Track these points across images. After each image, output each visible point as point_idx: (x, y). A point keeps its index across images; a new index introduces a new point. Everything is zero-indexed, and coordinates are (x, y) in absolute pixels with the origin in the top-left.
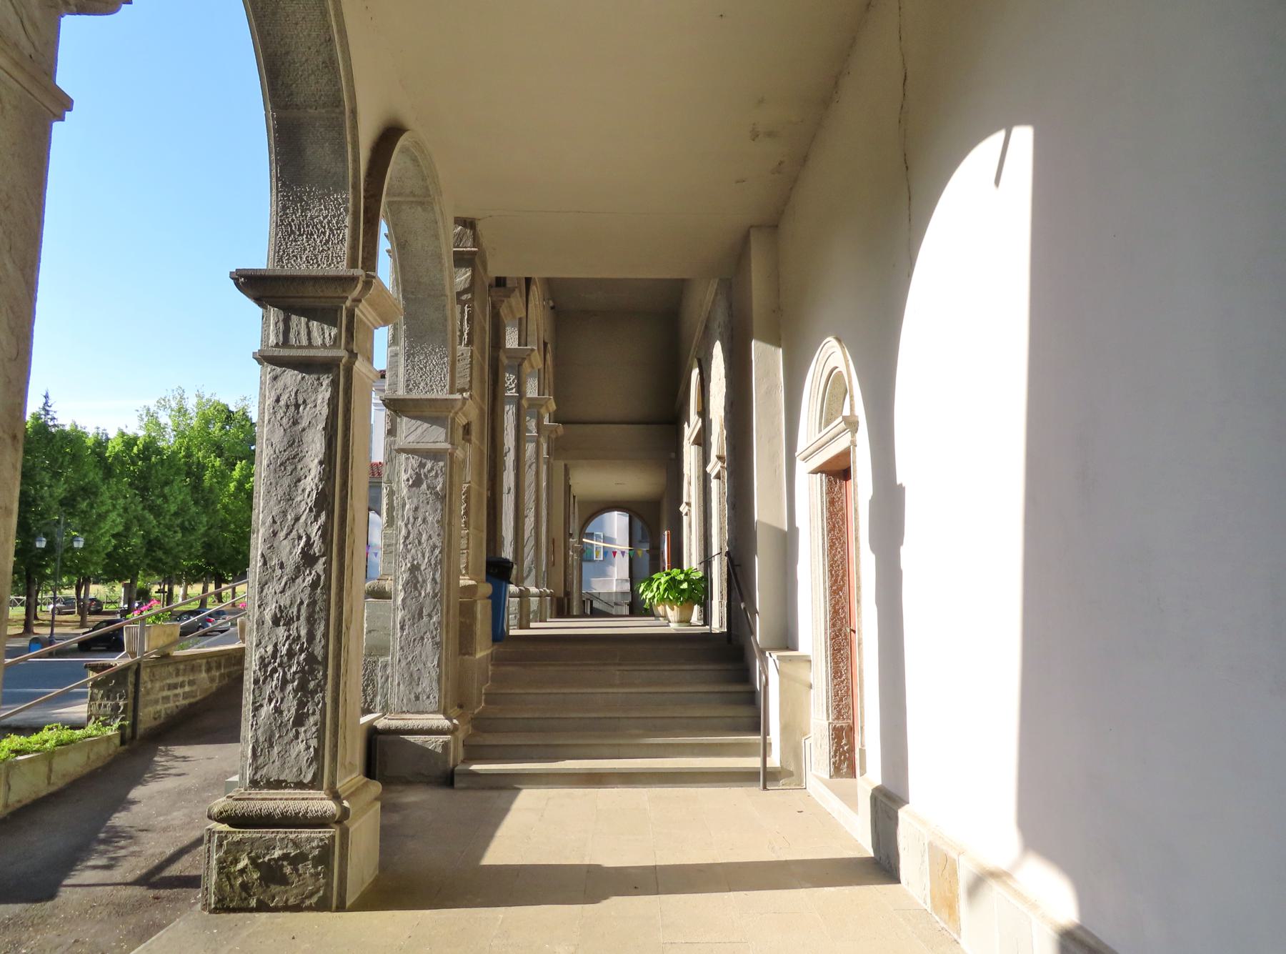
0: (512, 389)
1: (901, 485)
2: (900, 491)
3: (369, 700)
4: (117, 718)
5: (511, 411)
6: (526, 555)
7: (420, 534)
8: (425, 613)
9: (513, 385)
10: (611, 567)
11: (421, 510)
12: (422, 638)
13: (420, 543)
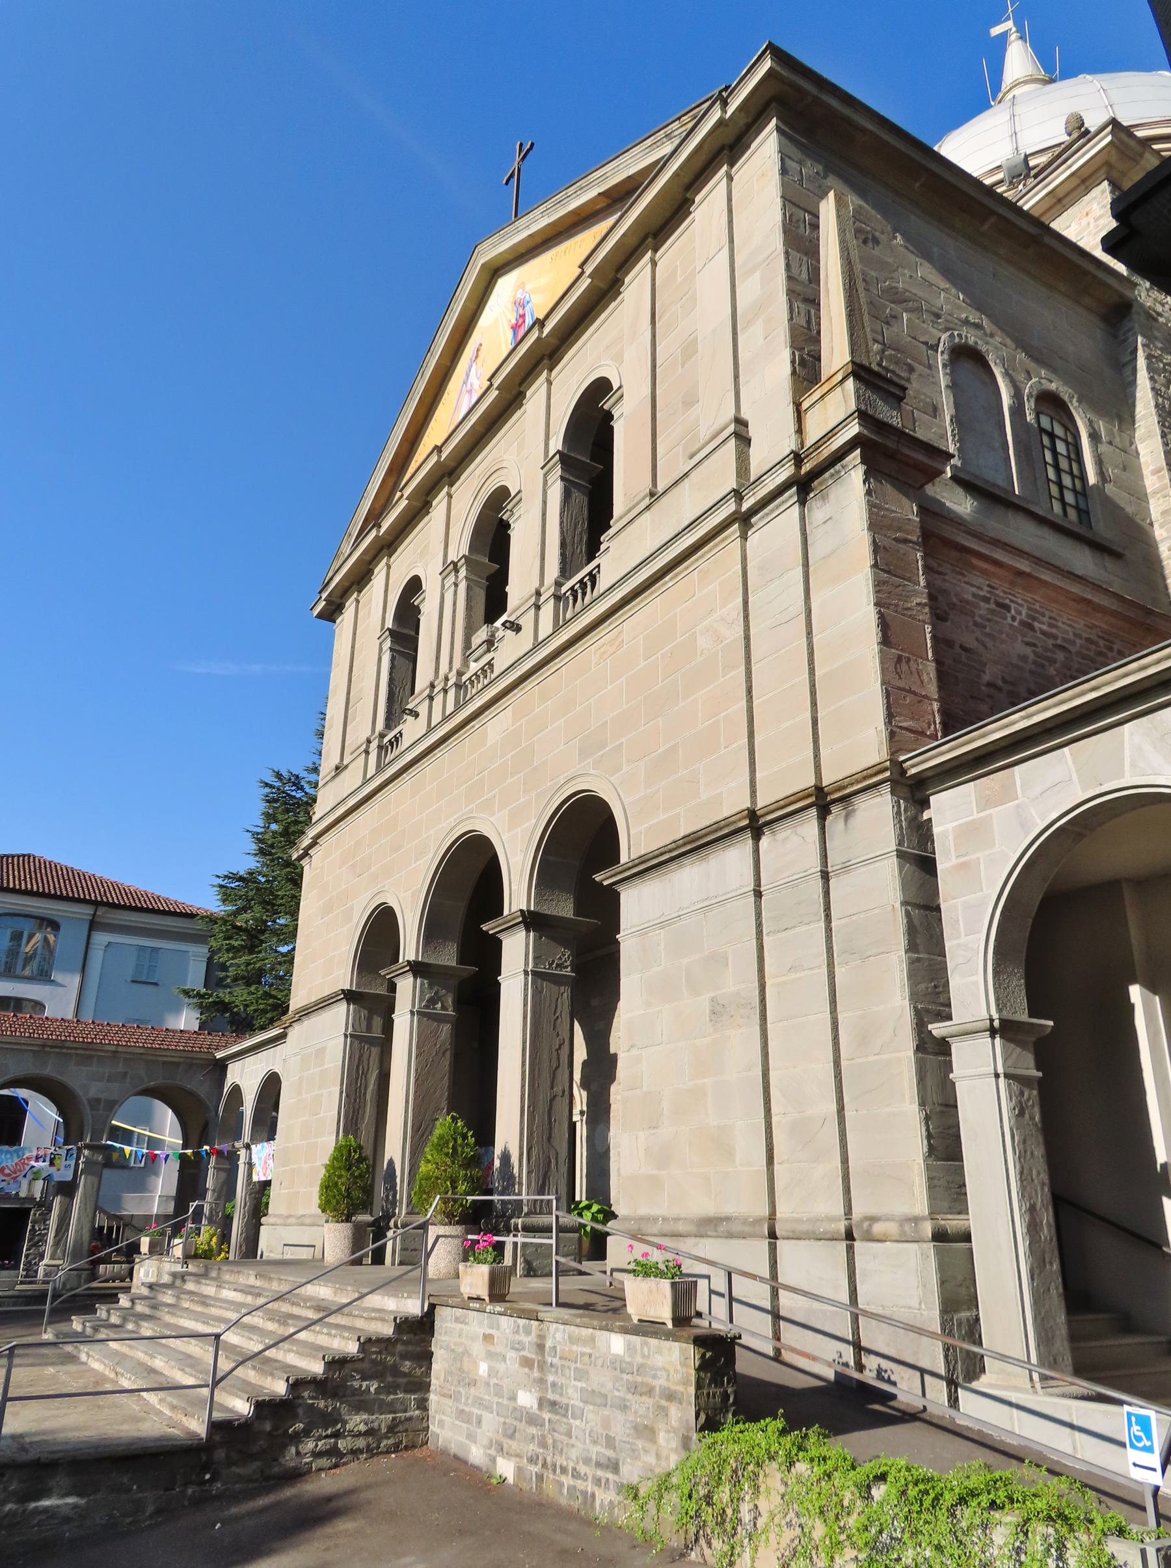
0: (567, 967)
1: (615, 1055)
2: (613, 1060)
3: (951, 1368)
4: (727, 1411)
5: (565, 994)
6: (516, 1171)
7: (1031, 1170)
8: (1047, 1260)
9: (568, 963)
10: (153, 1177)
11: (1029, 1142)
12: (1049, 1290)
13: (1032, 1180)
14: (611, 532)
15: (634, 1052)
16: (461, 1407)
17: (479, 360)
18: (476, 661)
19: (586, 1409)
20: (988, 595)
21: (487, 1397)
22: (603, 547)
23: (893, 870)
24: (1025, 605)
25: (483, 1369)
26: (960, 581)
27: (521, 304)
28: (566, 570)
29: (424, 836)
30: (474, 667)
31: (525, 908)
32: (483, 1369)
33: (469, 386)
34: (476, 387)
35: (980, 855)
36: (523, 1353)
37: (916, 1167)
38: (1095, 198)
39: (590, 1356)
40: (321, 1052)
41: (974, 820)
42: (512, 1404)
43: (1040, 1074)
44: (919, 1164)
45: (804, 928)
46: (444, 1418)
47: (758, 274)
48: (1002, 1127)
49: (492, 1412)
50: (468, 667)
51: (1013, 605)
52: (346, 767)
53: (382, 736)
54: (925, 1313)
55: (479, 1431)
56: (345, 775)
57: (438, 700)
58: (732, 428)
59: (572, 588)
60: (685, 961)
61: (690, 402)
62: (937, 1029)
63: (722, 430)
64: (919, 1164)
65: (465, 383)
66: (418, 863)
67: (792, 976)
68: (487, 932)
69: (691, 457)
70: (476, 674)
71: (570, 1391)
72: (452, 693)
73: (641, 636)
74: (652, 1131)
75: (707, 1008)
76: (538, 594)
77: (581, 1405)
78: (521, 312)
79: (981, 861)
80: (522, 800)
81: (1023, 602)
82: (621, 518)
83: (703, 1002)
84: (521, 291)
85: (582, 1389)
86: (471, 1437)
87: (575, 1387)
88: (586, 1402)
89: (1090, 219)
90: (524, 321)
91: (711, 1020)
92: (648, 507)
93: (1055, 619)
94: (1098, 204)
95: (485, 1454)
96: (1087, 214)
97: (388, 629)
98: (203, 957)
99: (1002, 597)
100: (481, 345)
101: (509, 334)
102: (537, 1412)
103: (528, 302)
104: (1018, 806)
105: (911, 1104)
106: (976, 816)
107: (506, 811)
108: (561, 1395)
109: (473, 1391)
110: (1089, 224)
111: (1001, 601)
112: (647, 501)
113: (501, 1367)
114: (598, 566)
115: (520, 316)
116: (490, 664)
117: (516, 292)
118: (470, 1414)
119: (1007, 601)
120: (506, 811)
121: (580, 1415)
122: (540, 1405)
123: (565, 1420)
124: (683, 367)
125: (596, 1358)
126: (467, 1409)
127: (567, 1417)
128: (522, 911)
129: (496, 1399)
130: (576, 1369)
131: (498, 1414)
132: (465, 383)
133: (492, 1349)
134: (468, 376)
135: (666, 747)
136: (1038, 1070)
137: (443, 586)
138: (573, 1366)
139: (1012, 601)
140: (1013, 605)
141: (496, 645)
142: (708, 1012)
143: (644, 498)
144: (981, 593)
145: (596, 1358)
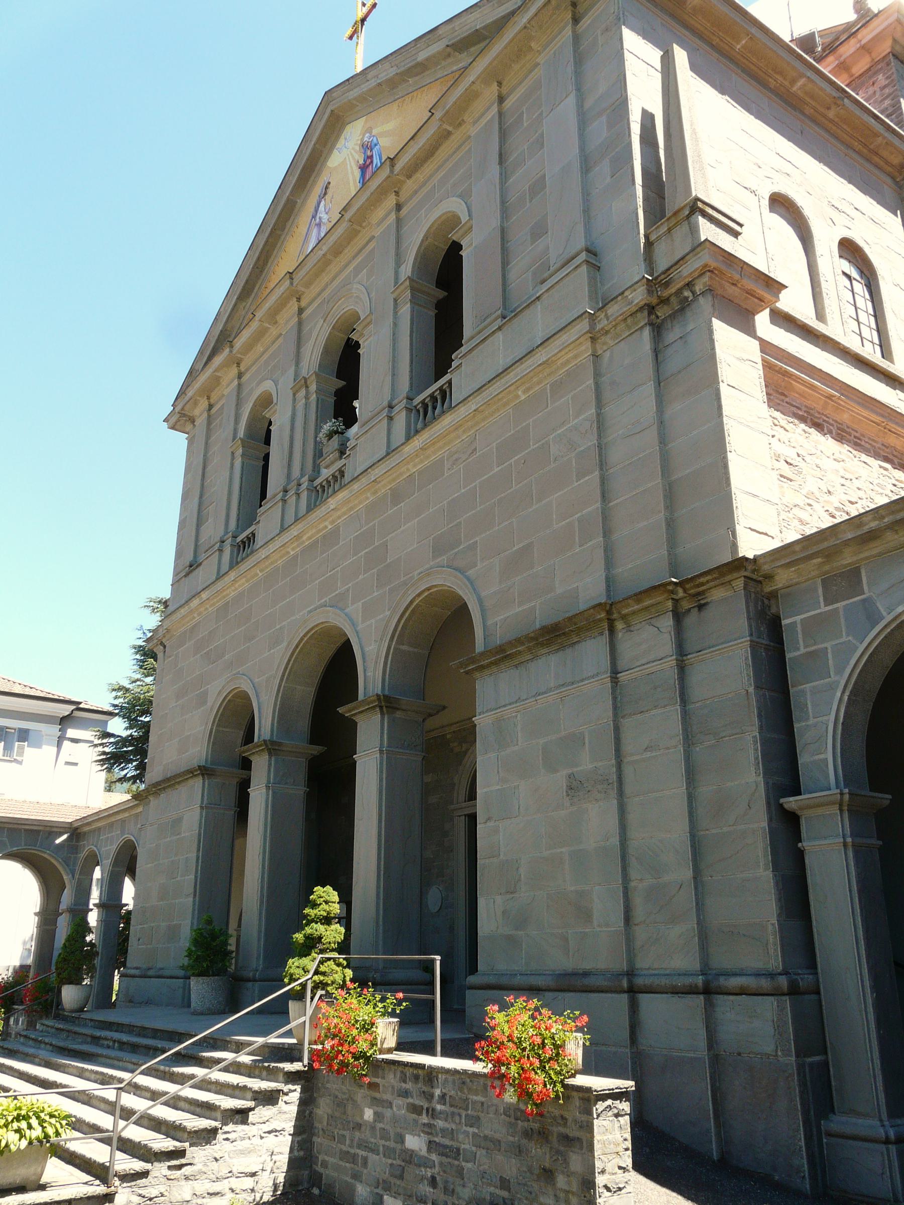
14: (463, 350)
15: (491, 824)
16: (344, 1148)
17: (326, 197)
18: (327, 467)
19: (478, 1153)
20: (805, 415)
21: (373, 1140)
22: (454, 365)
23: (747, 659)
24: (835, 424)
25: (368, 1114)
26: (783, 401)
27: (367, 147)
28: (417, 386)
29: (278, 627)
30: (326, 473)
31: (379, 693)
32: (368, 1114)
33: (318, 220)
34: (325, 220)
35: (828, 645)
36: (410, 1100)
37: (770, 928)
38: (881, 69)
39: (482, 1103)
40: (178, 821)
41: (821, 613)
42: (399, 1146)
43: (881, 843)
44: (773, 924)
45: (659, 711)
46: (327, 1158)
47: (604, 119)
48: (850, 891)
49: (378, 1154)
50: (319, 472)
51: (825, 425)
52: (200, 564)
53: (235, 537)
54: (780, 1059)
55: (365, 1171)
56: (200, 572)
57: (292, 501)
58: (583, 256)
59: (423, 402)
60: (542, 741)
61: (539, 231)
62: (791, 803)
63: (573, 258)
64: (773, 924)
65: (314, 217)
66: (272, 651)
67: (648, 754)
68: (343, 715)
69: (543, 282)
70: (327, 479)
71: (461, 1137)
72: (304, 496)
73: (495, 444)
74: (509, 896)
75: (564, 784)
76: (391, 407)
77: (474, 1149)
78: (369, 153)
79: (829, 651)
80: (376, 594)
81: (833, 423)
82: (472, 338)
83: (560, 778)
84: (367, 135)
85: (474, 1134)
86: (356, 1176)
87: (466, 1133)
88: (479, 1146)
89: (876, 88)
90: (372, 162)
91: (568, 795)
92: (500, 328)
93: (859, 439)
94: (883, 76)
95: (371, 1192)
96: (873, 84)
97: (240, 438)
98: (55, 736)
99: (816, 417)
100: (329, 183)
101: (357, 173)
102: (426, 1155)
103: (376, 145)
104: (864, 601)
105: (765, 870)
106: (824, 609)
107: (360, 604)
108: (452, 1139)
109: (357, 1134)
110: (875, 92)
111: (816, 420)
112: (499, 322)
113: (388, 1113)
114: (450, 383)
115: (368, 157)
116: (342, 473)
117: (364, 136)
118: (355, 1156)
119: (820, 421)
120: (360, 604)
121: (473, 1158)
122: (429, 1150)
123: (456, 1163)
124: (531, 201)
125: (488, 1107)
126: (352, 1151)
127: (458, 1160)
128: (377, 695)
129: (383, 1142)
130: (467, 1116)
131: (384, 1156)
132: (314, 217)
133: (377, 1095)
134: (316, 210)
135: (521, 545)
136: (879, 839)
137: (294, 400)
138: (464, 1114)
139: (824, 421)
140: (825, 425)
141: (348, 453)
142: (565, 787)
143: (496, 319)
144: (801, 413)
145: (488, 1107)
